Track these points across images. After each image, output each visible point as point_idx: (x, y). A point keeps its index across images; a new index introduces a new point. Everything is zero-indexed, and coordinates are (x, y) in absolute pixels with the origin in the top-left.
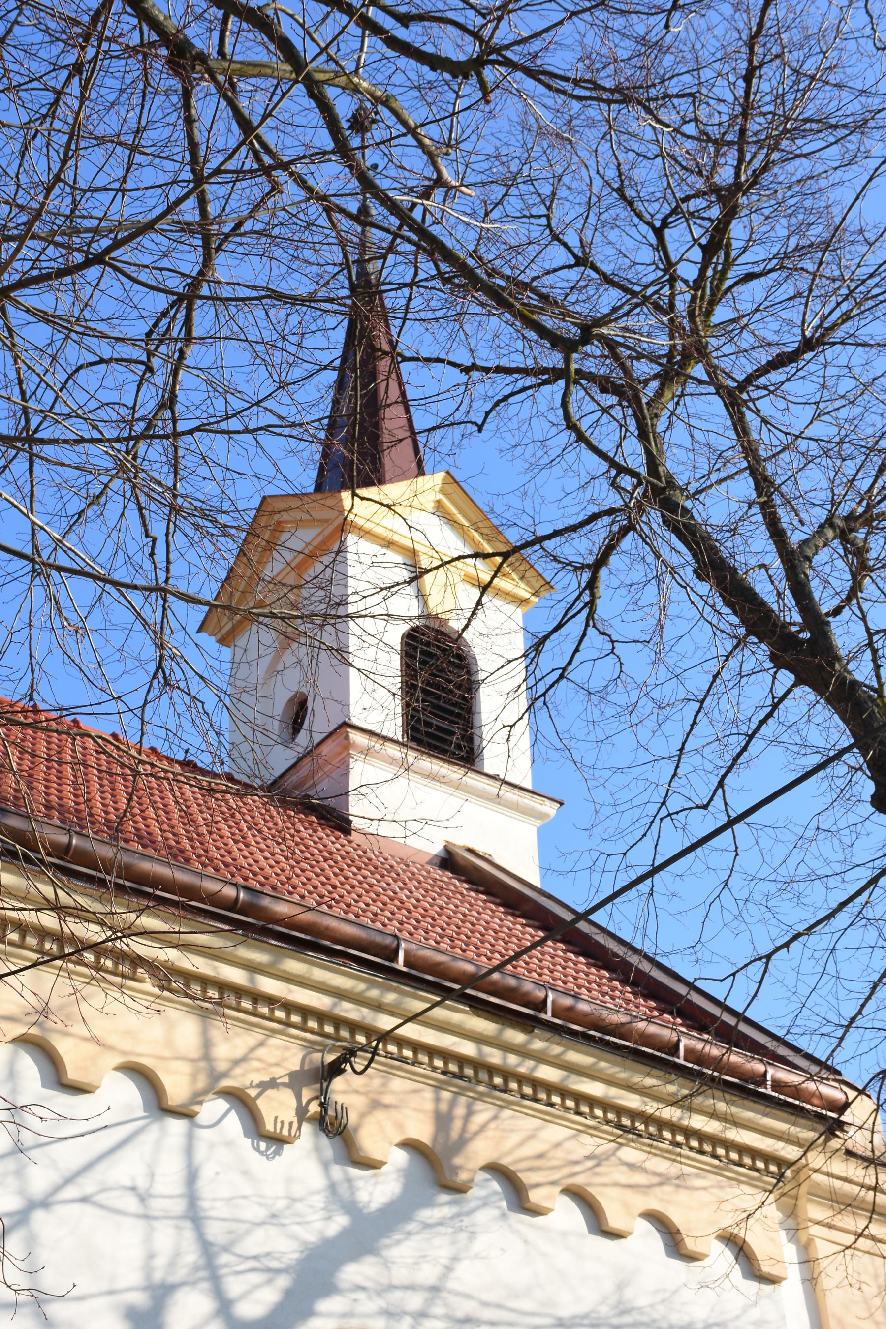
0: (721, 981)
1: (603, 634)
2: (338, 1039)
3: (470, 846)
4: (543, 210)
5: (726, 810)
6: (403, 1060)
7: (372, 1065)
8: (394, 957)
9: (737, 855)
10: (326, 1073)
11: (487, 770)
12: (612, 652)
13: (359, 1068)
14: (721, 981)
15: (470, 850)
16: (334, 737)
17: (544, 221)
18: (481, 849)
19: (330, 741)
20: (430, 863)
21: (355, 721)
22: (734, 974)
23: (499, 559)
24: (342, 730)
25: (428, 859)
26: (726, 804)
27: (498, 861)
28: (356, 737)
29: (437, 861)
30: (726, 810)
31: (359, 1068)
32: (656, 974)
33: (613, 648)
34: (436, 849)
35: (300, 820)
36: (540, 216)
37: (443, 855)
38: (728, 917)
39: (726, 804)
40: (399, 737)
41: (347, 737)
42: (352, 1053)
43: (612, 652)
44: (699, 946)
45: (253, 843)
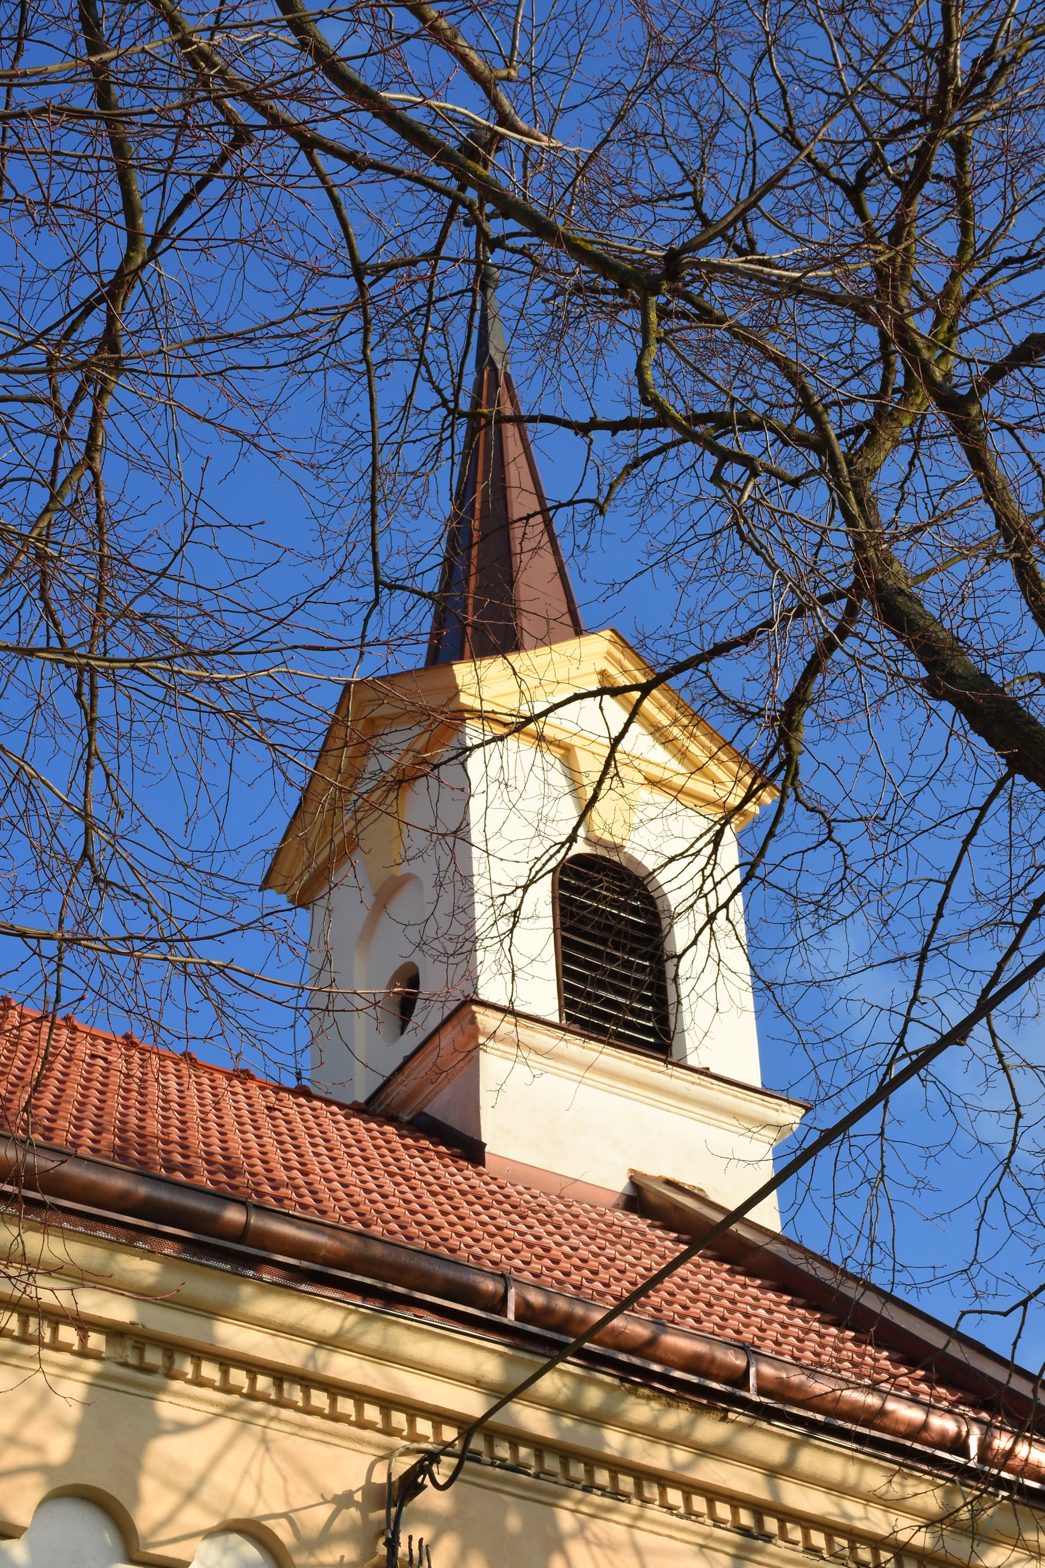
0: (1005, 1314)
1: (813, 810)
2: (414, 1437)
3: (670, 1176)
4: (688, 187)
5: (995, 1046)
6: (517, 1468)
7: (461, 1476)
8: (502, 1310)
9: (1019, 1116)
10: (395, 1493)
11: (691, 1061)
12: (830, 838)
13: (441, 1480)
14: (1005, 1314)
15: (669, 1183)
16: (455, 1021)
17: (689, 202)
18: (687, 1179)
19: (449, 1028)
20: (616, 1206)
21: (484, 994)
22: (1024, 1303)
23: (636, 695)
24: (465, 1011)
25: (614, 1199)
26: (993, 1035)
27: (713, 1198)
28: (487, 1020)
29: (621, 1203)
30: (995, 1046)
31: (441, 1480)
32: (955, 1350)
33: (830, 832)
34: (620, 1184)
35: (406, 1147)
36: (683, 196)
37: (629, 1192)
38: (1015, 1217)
39: (993, 1035)
40: (555, 1018)
41: (473, 1020)
42: (433, 1457)
43: (830, 838)
44: (975, 1269)
45: (318, 1171)
